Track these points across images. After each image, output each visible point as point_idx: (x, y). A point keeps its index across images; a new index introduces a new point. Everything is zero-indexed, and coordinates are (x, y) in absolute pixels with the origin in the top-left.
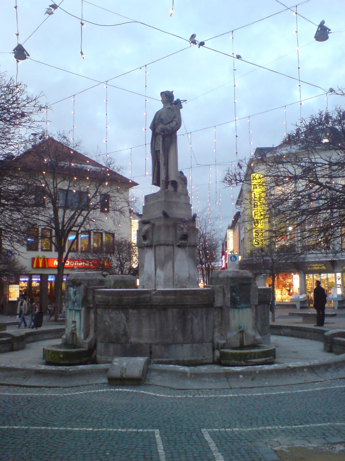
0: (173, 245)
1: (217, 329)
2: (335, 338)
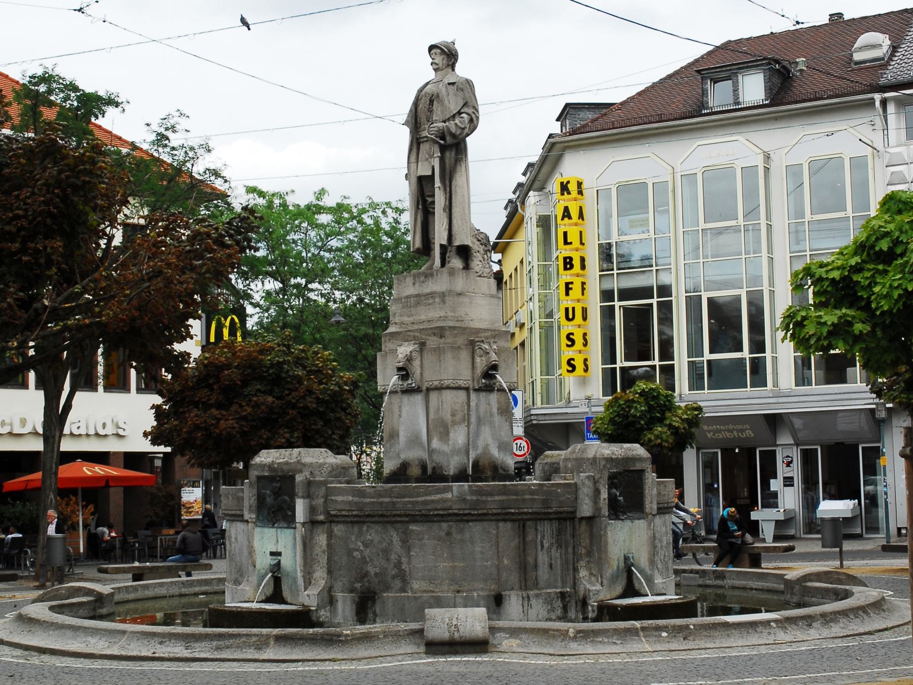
0: (467, 389)
1: (582, 563)
2: (809, 584)
